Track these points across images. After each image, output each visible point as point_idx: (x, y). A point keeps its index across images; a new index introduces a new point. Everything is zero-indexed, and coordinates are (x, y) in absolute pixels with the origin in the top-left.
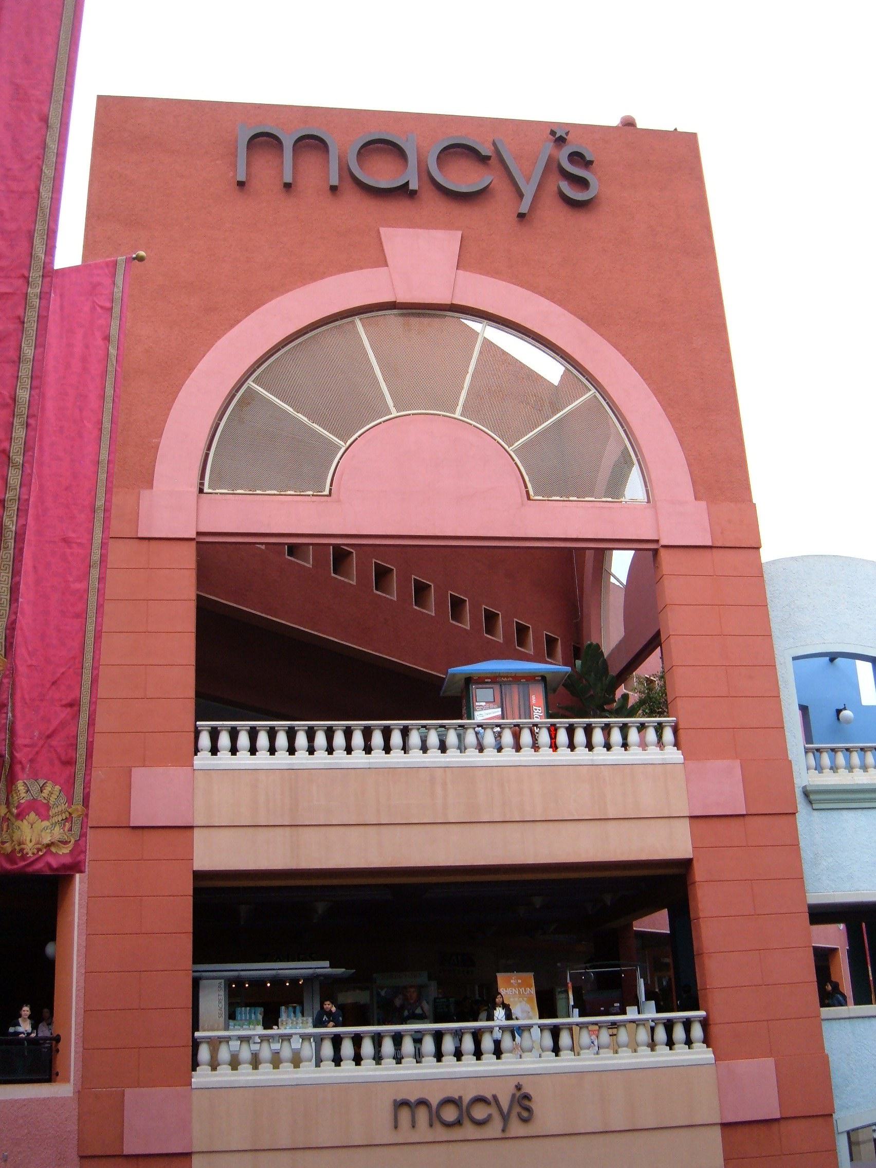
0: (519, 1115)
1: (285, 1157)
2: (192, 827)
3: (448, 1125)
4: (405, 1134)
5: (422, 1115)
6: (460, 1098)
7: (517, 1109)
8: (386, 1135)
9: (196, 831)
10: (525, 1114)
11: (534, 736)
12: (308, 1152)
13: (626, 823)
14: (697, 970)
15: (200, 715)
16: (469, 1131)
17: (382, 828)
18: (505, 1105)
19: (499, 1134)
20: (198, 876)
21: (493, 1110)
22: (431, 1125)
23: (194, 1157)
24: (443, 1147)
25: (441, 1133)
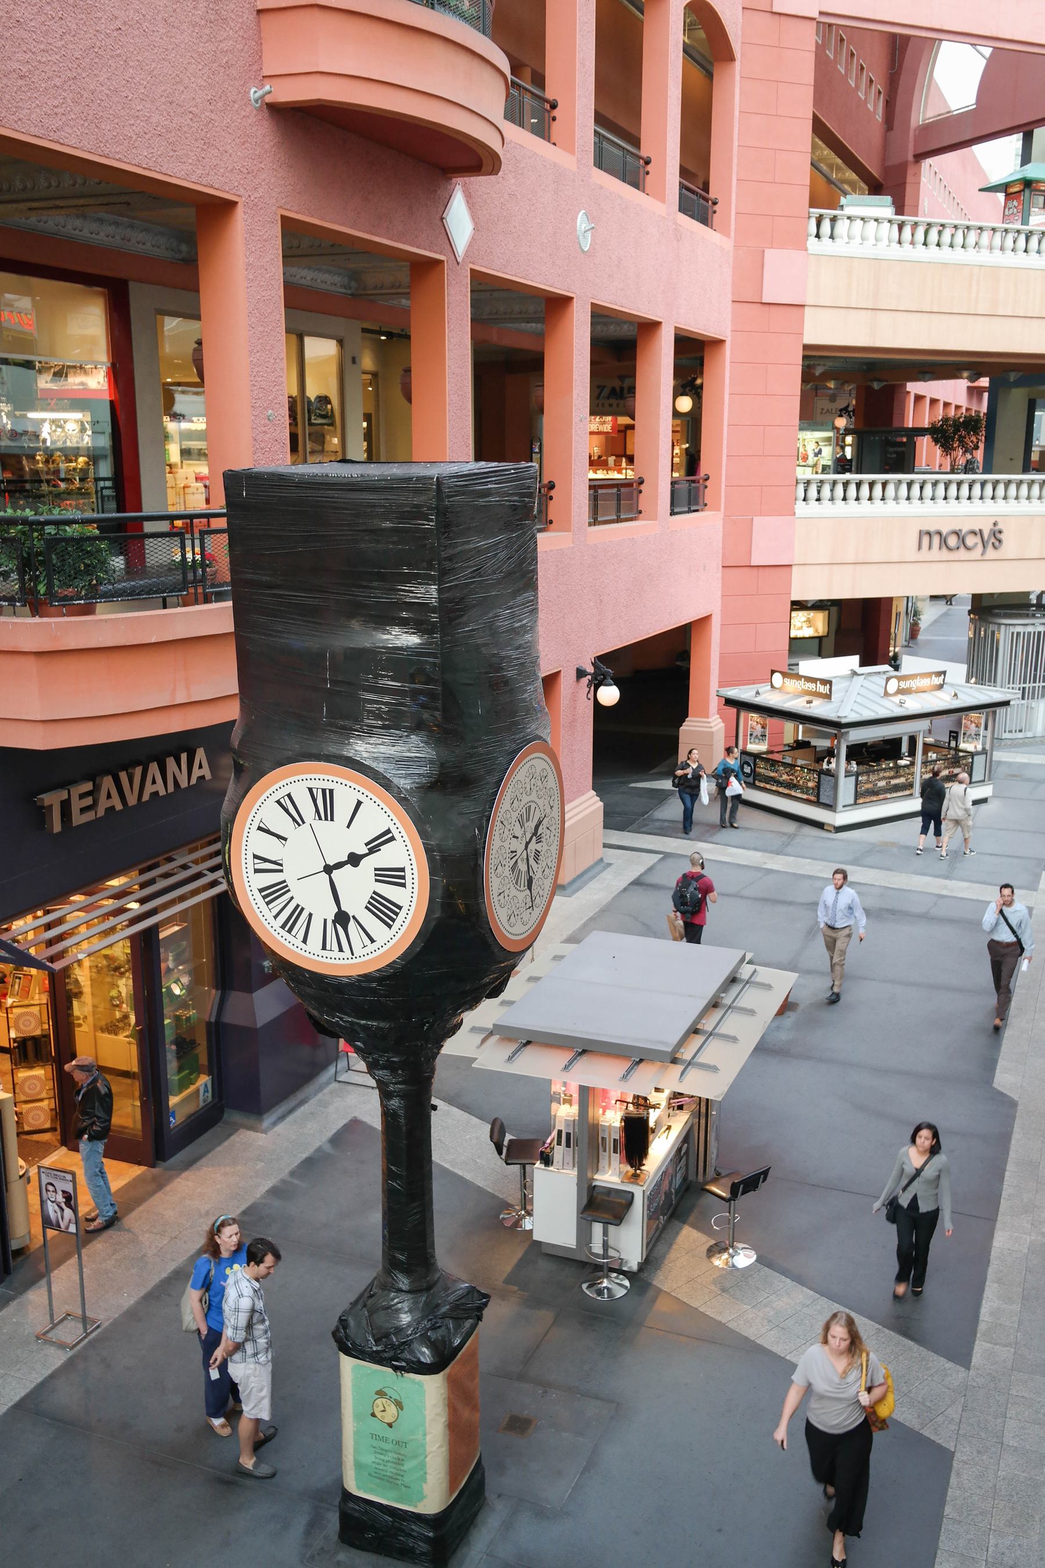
0: (993, 543)
1: (851, 566)
2: (803, 306)
3: (949, 549)
4: (925, 554)
5: (936, 540)
6: (960, 530)
7: (993, 540)
8: (912, 554)
9: (807, 309)
10: (997, 543)
11: (897, 489)
12: (864, 566)
13: (917, 564)
14: (460, 1173)
15: (813, 204)
16: (962, 554)
17: (933, 315)
18: (986, 536)
19: (979, 557)
20: (806, 347)
21: (978, 539)
22: (940, 549)
23: (794, 568)
24: (944, 565)
25: (945, 554)
